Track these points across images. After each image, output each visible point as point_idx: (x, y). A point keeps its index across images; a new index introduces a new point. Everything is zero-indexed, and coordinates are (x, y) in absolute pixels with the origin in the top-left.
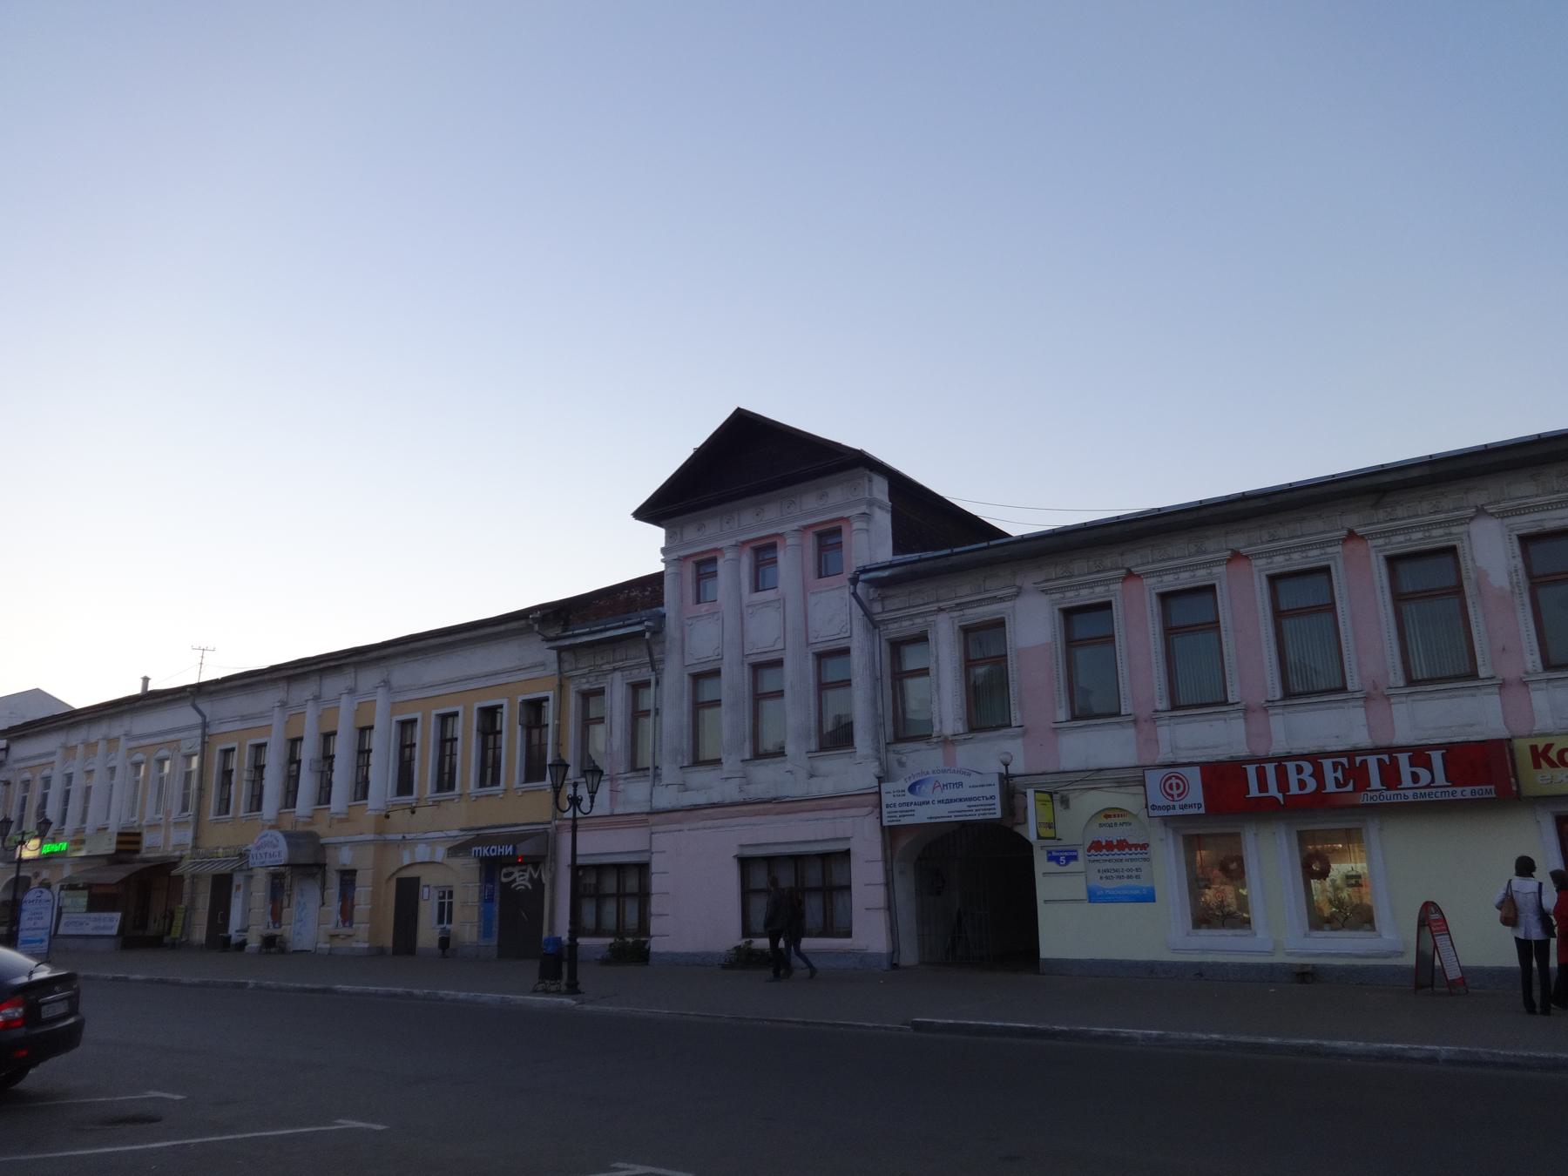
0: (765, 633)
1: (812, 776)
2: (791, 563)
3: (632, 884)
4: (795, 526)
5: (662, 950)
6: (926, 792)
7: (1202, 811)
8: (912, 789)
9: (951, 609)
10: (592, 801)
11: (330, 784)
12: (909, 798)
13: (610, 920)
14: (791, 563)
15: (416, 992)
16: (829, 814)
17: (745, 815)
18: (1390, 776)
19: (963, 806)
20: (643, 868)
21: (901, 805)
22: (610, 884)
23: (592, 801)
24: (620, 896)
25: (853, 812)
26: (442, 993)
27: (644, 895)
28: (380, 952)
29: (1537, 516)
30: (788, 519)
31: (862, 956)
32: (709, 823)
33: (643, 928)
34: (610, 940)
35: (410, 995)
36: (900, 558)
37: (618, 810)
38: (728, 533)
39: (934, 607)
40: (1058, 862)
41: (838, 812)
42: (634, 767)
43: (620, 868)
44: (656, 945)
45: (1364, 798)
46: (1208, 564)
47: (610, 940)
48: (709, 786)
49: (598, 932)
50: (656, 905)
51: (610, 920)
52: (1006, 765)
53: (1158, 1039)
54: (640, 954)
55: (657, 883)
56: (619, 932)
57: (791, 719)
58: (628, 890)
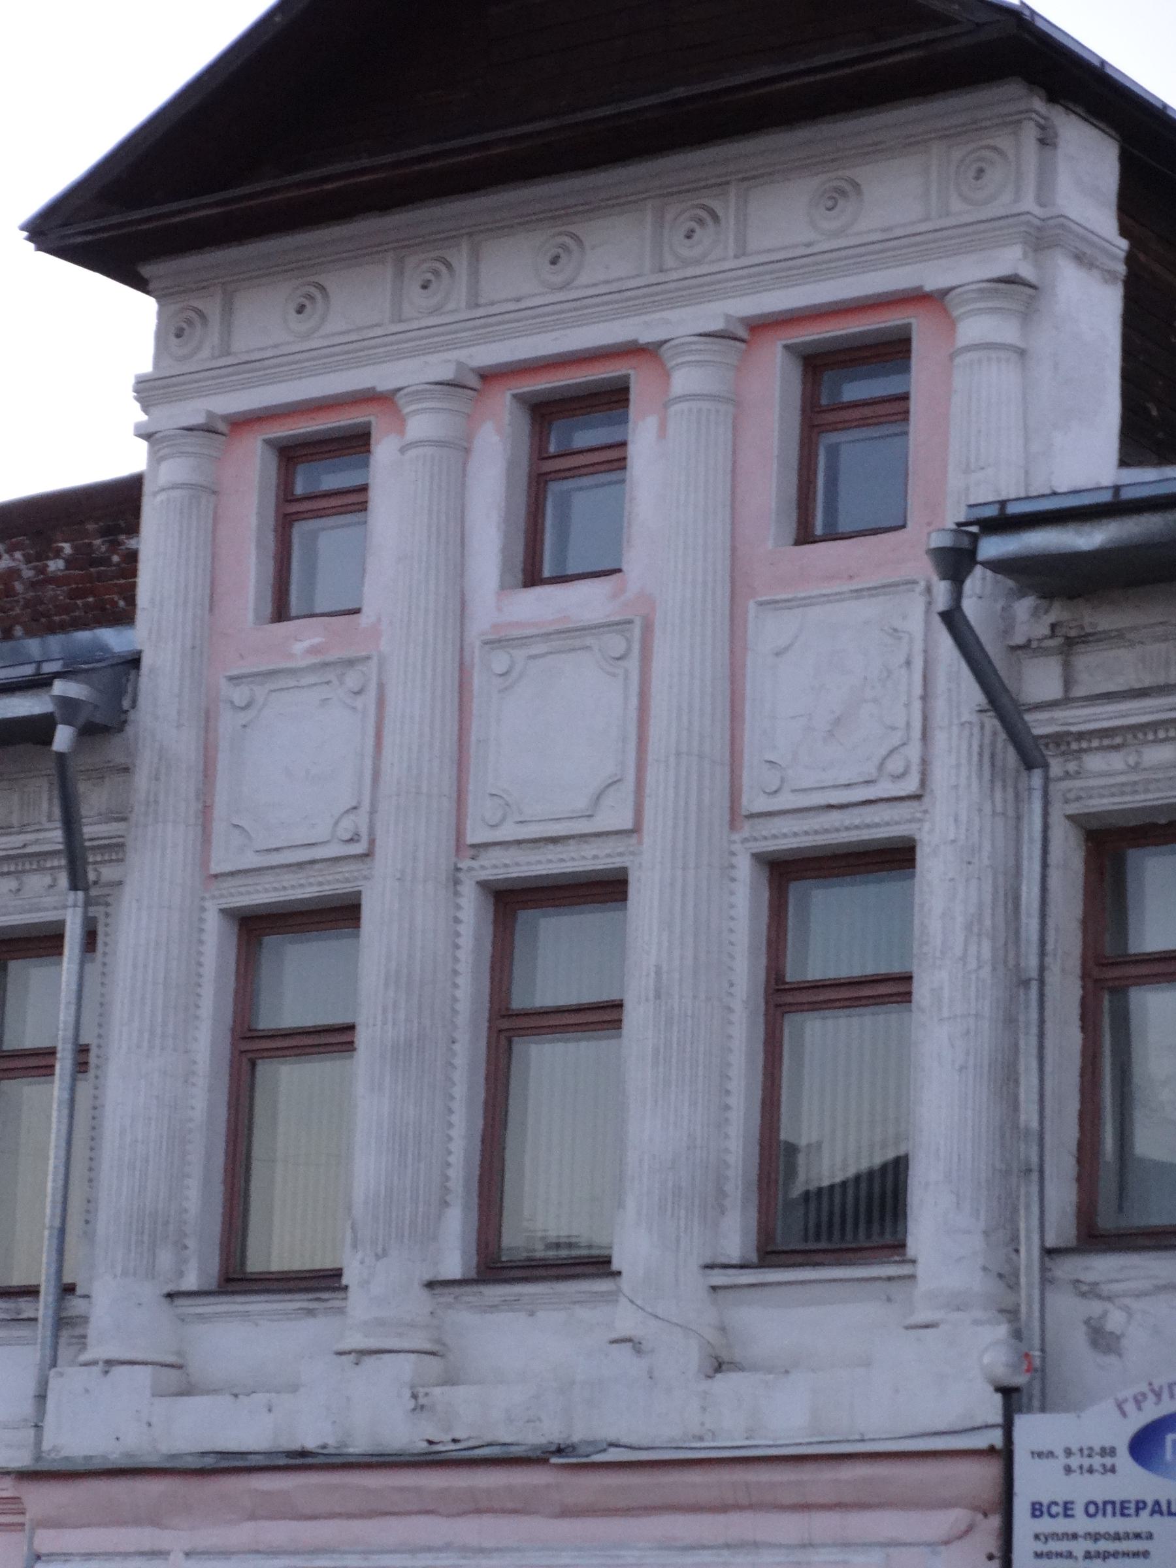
0: (559, 756)
14: (691, 468)
41: (823, 1524)
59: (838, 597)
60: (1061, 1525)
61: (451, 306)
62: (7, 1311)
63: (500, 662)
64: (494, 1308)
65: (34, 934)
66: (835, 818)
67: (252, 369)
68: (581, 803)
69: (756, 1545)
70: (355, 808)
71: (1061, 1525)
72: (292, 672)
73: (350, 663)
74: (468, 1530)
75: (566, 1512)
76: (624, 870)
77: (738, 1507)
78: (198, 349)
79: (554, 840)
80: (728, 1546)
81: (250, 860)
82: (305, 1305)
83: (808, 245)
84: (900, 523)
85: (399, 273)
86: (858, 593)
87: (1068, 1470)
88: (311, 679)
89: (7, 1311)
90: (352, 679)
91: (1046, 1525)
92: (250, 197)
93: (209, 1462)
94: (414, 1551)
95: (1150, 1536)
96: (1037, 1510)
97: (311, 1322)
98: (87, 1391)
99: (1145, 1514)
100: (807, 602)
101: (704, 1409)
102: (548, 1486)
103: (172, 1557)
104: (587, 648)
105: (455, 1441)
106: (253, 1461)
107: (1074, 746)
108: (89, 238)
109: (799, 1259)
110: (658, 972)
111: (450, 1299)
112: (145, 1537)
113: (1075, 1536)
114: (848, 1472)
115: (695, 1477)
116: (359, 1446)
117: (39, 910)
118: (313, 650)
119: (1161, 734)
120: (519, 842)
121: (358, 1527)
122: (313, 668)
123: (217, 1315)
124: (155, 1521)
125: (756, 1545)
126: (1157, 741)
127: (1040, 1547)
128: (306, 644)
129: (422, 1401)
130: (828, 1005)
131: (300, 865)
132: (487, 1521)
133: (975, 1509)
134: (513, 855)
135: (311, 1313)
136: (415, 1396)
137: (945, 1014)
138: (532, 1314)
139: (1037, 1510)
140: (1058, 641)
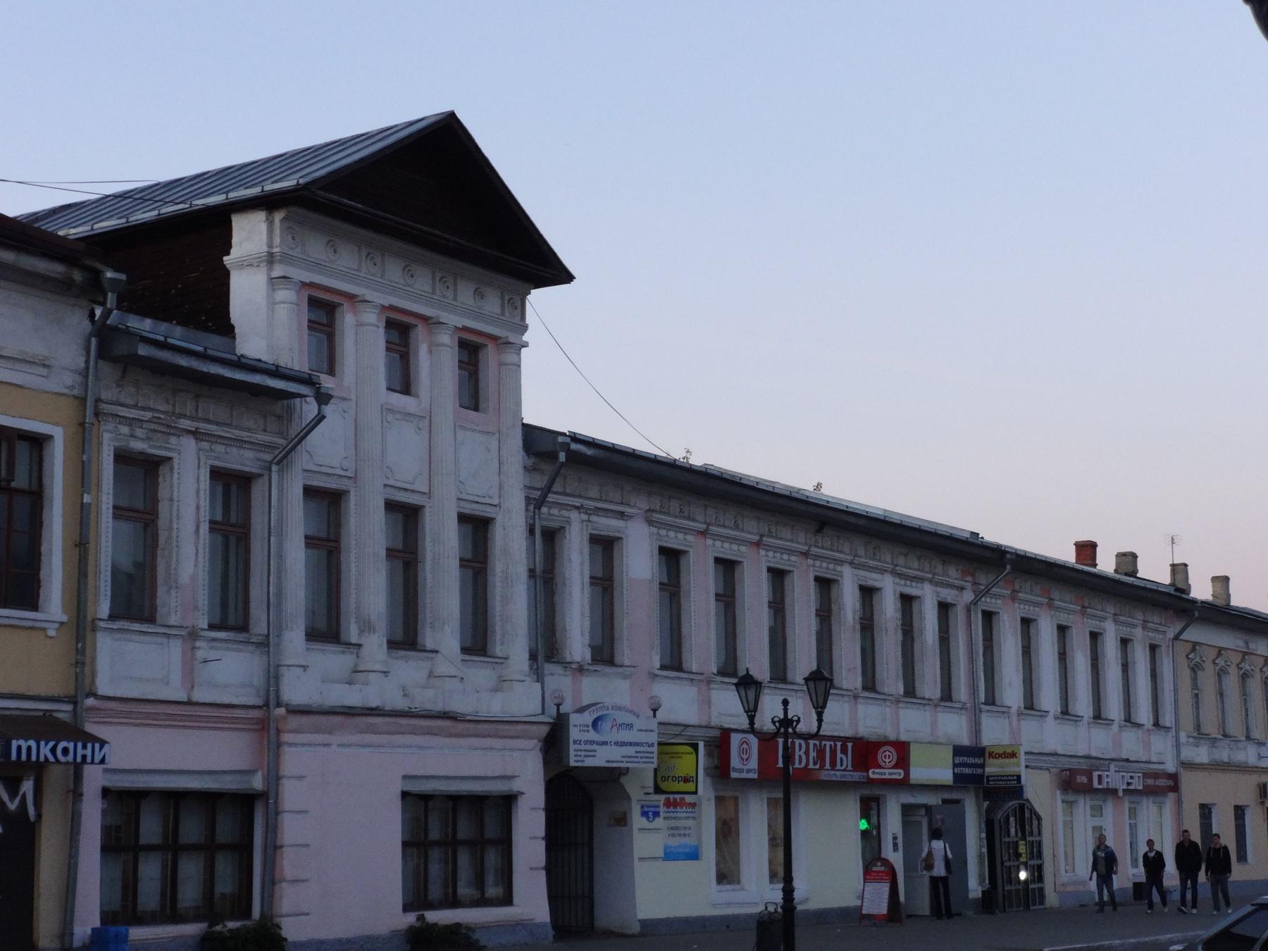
2: (436, 363)
3: (226, 830)
4: (308, 277)
6: (606, 725)
7: (755, 776)
8: (595, 724)
12: (592, 735)
13: (189, 893)
14: (436, 363)
16: (497, 743)
17: (414, 732)
18: (903, 761)
21: (586, 742)
24: (209, 849)
32: (369, 738)
34: (192, 929)
36: (1118, 576)
37: (198, 696)
38: (377, 283)
39: (577, 502)
40: (648, 818)
42: (1225, 736)
45: (825, 775)
46: (686, 531)
48: (395, 681)
49: (170, 913)
51: (189, 893)
52: (558, 705)
53: (1123, 945)
56: (208, 910)
59: (474, 431)
66: (475, 506)
67: (316, 266)
75: (450, 735)
91: (577, 747)
96: (575, 742)
135: (343, 652)
139: (575, 742)
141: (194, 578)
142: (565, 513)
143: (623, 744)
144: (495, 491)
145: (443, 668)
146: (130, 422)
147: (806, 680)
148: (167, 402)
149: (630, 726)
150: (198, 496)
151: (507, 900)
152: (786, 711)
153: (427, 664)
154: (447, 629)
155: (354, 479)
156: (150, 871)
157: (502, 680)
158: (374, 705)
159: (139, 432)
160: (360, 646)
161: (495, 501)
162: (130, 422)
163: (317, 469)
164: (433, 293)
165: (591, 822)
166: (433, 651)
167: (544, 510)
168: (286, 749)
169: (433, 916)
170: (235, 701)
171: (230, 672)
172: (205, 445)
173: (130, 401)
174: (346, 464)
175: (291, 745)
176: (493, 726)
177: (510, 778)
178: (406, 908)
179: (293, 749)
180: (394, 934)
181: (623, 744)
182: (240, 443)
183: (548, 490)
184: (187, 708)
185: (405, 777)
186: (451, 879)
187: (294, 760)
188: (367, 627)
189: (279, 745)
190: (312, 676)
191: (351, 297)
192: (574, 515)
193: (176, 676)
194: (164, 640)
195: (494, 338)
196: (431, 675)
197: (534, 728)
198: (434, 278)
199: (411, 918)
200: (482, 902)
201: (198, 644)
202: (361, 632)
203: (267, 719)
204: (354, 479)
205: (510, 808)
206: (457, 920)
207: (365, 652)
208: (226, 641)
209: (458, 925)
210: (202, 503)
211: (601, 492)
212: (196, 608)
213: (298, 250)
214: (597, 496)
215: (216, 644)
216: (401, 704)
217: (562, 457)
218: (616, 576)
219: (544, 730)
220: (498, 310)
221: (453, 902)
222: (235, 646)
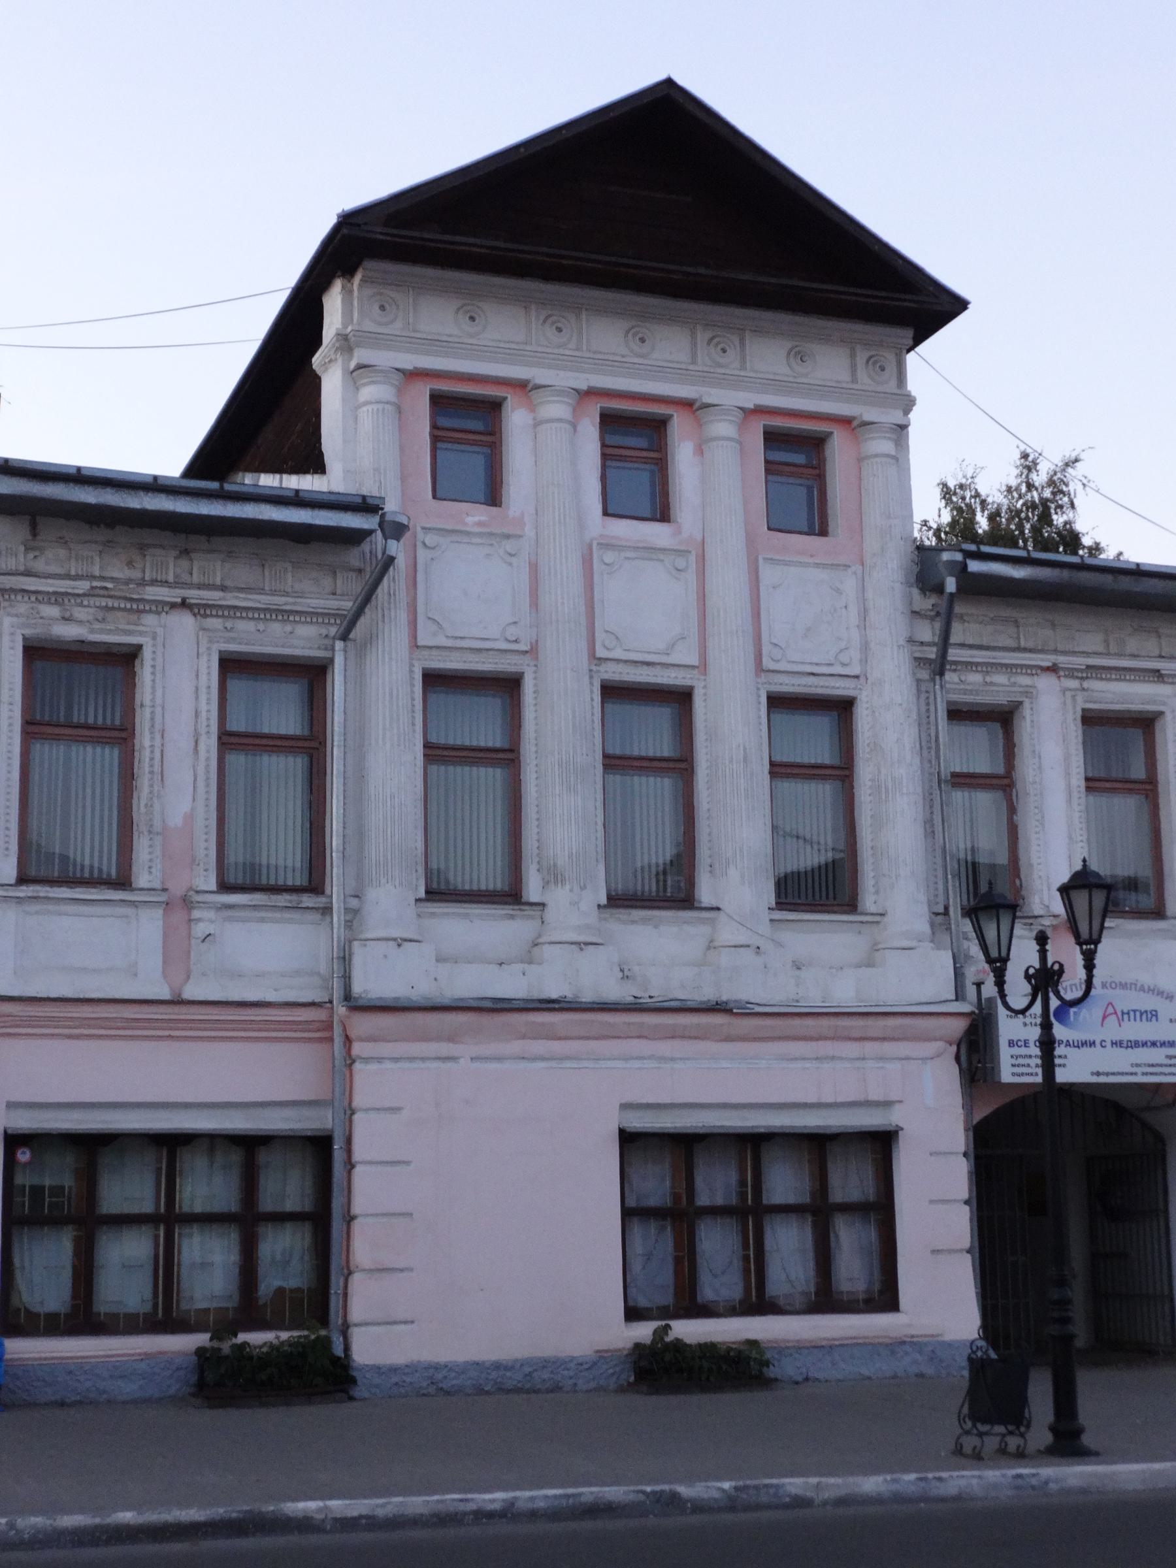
0: (648, 621)
1: (136, 975)
2: (716, 474)
5: (397, 1356)
9: (1071, 673)
10: (1089, 966)
11: (218, 810)
14: (716, 474)
15: (683, 1490)
19: (1158, 1055)
20: (320, 1152)
22: (784, 1182)
23: (1089, 966)
25: (903, 1048)
26: (795, 1485)
27: (322, 1220)
28: (629, 1384)
29: (939, 714)
30: (729, 378)
31: (930, 1349)
33: (318, 1300)
34: (201, 1339)
35: (672, 1502)
37: (190, 993)
38: (554, 361)
39: (1046, 660)
41: (870, 1048)
43: (818, 1146)
44: (368, 1349)
47: (201, 1339)
49: (165, 1317)
50: (365, 1245)
54: (317, 1373)
55: (368, 1190)
57: (741, 829)
58: (703, 1199)
59: (807, 565)
60: (1023, 1051)
61: (570, 346)
62: (290, 901)
63: (609, 557)
64: (633, 922)
65: (289, 662)
66: (812, 680)
67: (434, 344)
68: (661, 646)
69: (833, 1058)
70: (515, 623)
71: (1023, 1051)
72: (468, 533)
73: (508, 537)
74: (665, 1048)
75: (729, 1039)
76: (692, 688)
77: (826, 1038)
78: (392, 322)
79: (648, 664)
80: (817, 1059)
81: (442, 641)
82: (511, 912)
83: (623, 356)
84: (438, 495)
85: (853, 356)
86: (817, 565)
87: (1025, 1024)
88: (479, 540)
89: (290, 901)
90: (509, 546)
91: (1016, 1051)
92: (867, 296)
93: (489, 1004)
94: (626, 1059)
95: (1066, 1057)
96: (1011, 1043)
97: (511, 922)
98: (385, 956)
99: (1062, 1046)
100: (787, 563)
101: (797, 985)
102: (722, 1025)
103: (462, 1061)
104: (662, 561)
105: (651, 997)
106: (516, 1005)
107: (291, 618)
108: (389, 238)
109: (792, 907)
110: (745, 749)
111: (607, 916)
112: (444, 1048)
113: (1030, 1056)
114: (892, 1022)
115: (810, 1022)
116: (587, 997)
117: (290, 647)
118: (480, 524)
119: (303, 619)
120: (626, 661)
121: (593, 1045)
122: (481, 535)
123: (447, 914)
124: (451, 1039)
125: (833, 1058)
126: (1026, 674)
127: (1014, 1061)
128: (476, 519)
129: (626, 973)
130: (795, 776)
131: (479, 650)
132: (677, 1043)
133: (947, 1042)
134: (620, 668)
135: (512, 917)
136: (622, 970)
137: (905, 791)
138: (656, 927)
139: (1011, 1043)
140: (933, 613)
141: (190, 818)
142: (1025, 680)
143: (1135, 1044)
144: (855, 654)
145: (728, 933)
146: (57, 598)
147: (1064, 890)
148: (130, 564)
149: (1153, 1015)
150: (197, 698)
151: (885, 1296)
152: (1043, 953)
153: (705, 930)
154: (733, 873)
155: (533, 651)
156: (717, 1245)
157: (875, 948)
158: (554, 996)
159: (80, 613)
160: (543, 905)
161: (856, 670)
162: (57, 598)
163: (449, 643)
164: (694, 362)
165: (1165, 1173)
166: (712, 909)
167: (948, 676)
168: (358, 1066)
169: (689, 1330)
170: (271, 997)
171: (267, 952)
172: (214, 623)
173: (55, 569)
174: (512, 632)
175: (367, 1060)
176: (833, 1021)
177: (887, 1104)
178: (633, 1314)
179: (373, 1067)
180: (602, 1356)
181: (1135, 1044)
182: (284, 615)
183: (944, 643)
184: (176, 1009)
185: (625, 1107)
186: (755, 1263)
187: (372, 1084)
188: (553, 877)
189: (350, 1061)
190: (409, 950)
191: (522, 386)
192: (1045, 683)
193: (152, 962)
194: (129, 911)
195: (846, 422)
196: (711, 946)
197: (942, 1021)
198: (694, 345)
199: (644, 1331)
200: (825, 1300)
201: (196, 914)
202: (546, 884)
203: (337, 1018)
204: (533, 651)
205: (891, 1151)
206: (752, 1336)
207: (549, 914)
208: (255, 907)
209: (753, 1344)
210: (203, 707)
211: (1106, 642)
212: (193, 861)
213: (399, 324)
214: (1101, 648)
215: (230, 913)
216: (615, 991)
217: (951, 585)
218: (1161, 778)
219: (958, 1027)
220: (845, 376)
221: (758, 1303)
222: (278, 915)
